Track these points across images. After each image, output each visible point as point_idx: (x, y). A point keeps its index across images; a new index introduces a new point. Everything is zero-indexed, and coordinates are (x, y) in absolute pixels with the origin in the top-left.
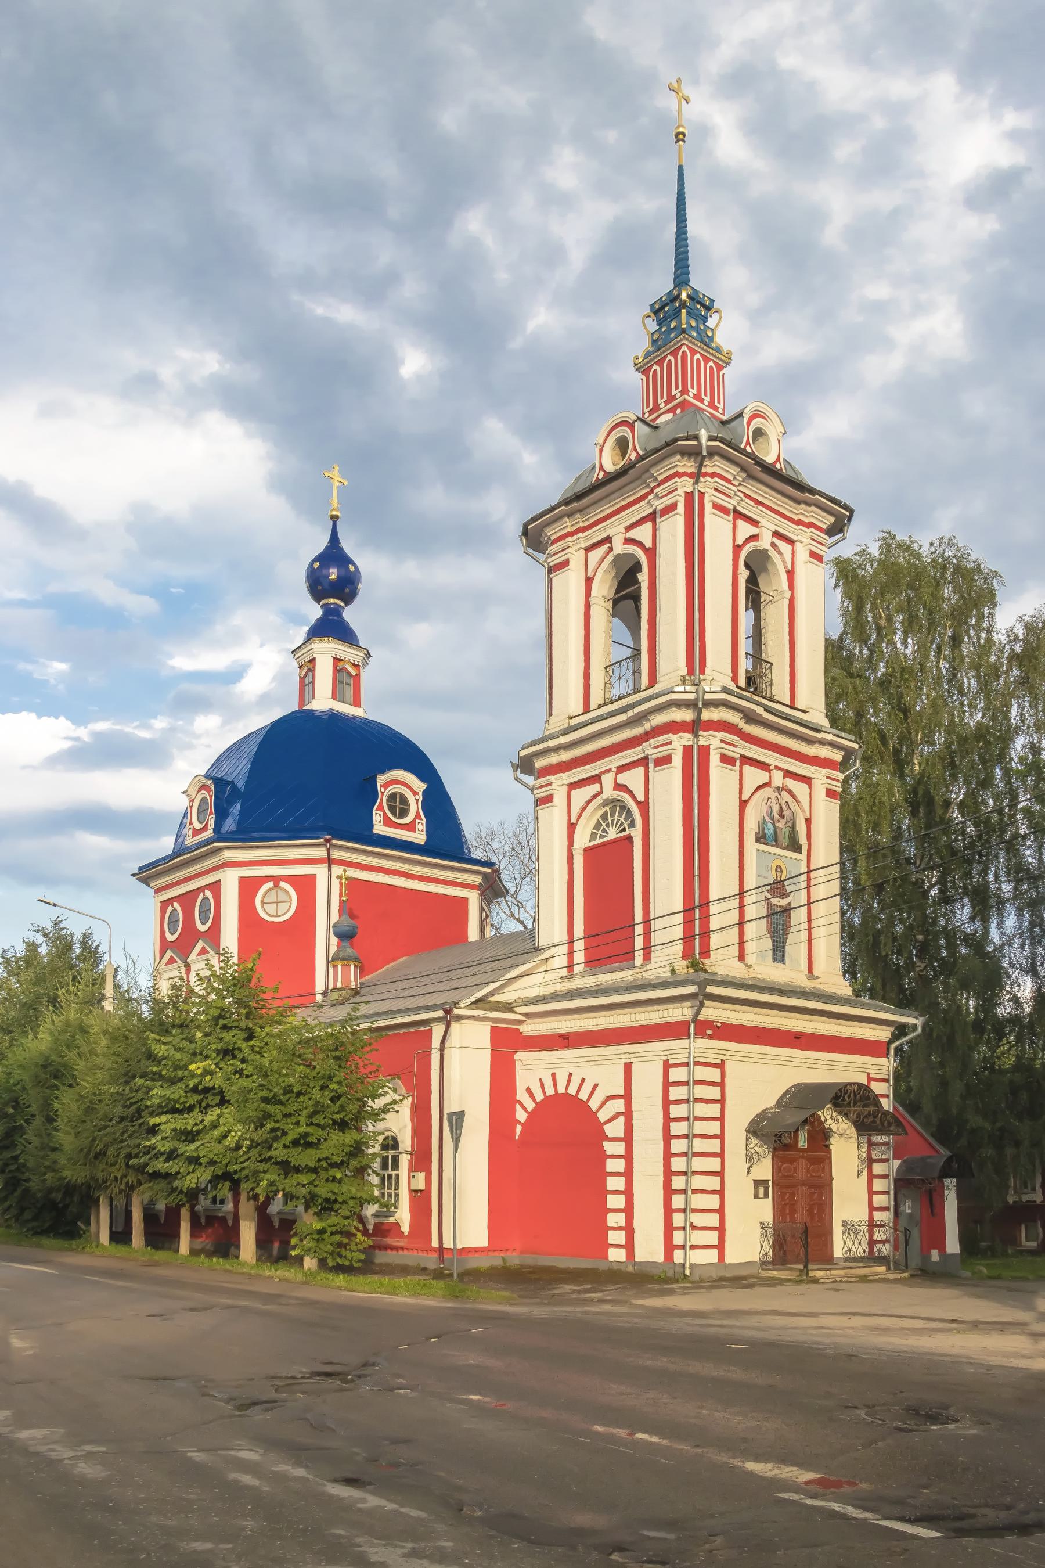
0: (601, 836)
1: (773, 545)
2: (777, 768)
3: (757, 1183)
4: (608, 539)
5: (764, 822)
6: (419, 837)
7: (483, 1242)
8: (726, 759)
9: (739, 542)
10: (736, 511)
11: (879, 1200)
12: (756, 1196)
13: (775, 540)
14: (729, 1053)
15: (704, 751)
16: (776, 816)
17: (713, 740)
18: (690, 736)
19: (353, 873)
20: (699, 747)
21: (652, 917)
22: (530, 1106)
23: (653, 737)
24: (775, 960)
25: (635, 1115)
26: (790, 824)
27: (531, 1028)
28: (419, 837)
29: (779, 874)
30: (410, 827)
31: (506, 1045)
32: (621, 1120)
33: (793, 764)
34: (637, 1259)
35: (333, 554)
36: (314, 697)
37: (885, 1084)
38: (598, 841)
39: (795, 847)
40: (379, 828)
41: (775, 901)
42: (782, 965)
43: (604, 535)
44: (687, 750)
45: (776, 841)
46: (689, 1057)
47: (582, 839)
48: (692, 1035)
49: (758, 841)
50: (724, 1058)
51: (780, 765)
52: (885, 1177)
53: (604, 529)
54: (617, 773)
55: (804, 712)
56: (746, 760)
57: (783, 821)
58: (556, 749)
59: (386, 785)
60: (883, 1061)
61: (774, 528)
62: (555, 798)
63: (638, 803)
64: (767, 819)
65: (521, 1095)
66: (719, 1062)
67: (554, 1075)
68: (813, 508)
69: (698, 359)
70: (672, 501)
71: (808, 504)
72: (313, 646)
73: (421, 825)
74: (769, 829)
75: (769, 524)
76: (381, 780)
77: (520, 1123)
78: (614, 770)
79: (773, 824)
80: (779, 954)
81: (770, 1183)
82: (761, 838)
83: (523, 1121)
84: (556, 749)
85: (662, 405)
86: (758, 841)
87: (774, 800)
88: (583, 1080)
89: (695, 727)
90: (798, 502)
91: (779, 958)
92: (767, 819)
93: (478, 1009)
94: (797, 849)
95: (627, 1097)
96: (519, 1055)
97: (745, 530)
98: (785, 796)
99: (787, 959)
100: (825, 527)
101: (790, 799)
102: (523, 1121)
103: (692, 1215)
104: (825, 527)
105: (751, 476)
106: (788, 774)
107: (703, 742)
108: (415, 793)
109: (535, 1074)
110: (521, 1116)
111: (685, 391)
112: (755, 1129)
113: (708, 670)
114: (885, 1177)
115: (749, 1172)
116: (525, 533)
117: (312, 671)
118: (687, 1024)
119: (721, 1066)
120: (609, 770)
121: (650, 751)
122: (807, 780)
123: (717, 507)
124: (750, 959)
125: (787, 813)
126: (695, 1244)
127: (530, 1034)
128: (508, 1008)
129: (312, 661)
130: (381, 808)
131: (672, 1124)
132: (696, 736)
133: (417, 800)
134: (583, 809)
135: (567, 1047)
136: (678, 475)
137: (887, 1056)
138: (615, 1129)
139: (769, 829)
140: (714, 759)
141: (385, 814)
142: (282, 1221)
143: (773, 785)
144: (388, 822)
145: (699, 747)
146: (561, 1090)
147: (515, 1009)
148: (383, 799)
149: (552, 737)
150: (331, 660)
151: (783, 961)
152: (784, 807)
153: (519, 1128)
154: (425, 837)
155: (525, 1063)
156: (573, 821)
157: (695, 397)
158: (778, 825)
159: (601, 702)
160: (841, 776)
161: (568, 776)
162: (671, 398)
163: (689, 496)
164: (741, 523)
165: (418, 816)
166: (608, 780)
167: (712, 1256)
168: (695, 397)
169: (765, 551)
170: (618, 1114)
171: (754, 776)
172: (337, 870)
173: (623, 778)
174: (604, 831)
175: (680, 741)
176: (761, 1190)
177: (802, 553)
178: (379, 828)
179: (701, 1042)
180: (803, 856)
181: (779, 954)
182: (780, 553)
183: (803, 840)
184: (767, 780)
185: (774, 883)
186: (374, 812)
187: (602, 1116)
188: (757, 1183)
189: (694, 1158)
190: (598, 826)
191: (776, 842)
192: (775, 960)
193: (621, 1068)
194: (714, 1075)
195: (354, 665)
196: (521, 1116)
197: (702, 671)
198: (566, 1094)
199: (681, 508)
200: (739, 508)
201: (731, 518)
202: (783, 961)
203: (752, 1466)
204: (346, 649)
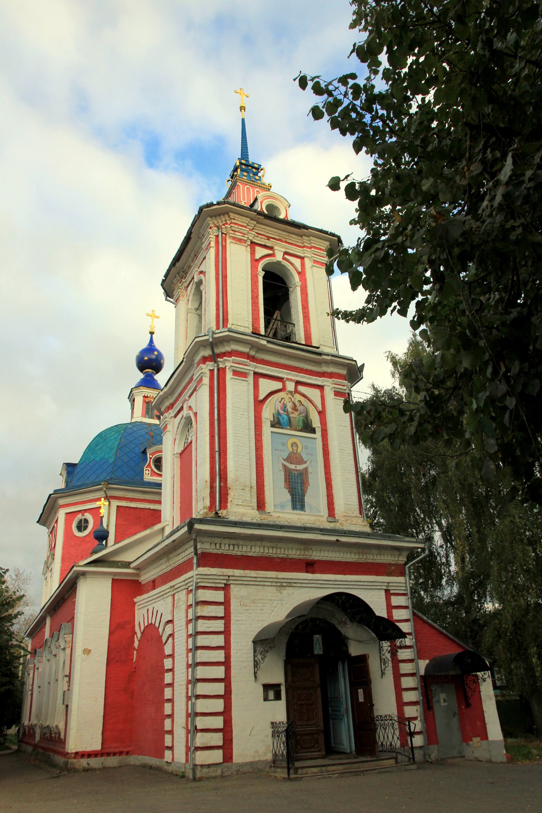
1: (284, 258)
2: (291, 380)
3: (267, 687)
5: (279, 413)
10: (252, 242)
11: (408, 697)
12: (266, 699)
13: (286, 256)
15: (222, 372)
16: (290, 410)
17: (228, 363)
19: (124, 504)
20: (219, 370)
24: (294, 508)
26: (303, 415)
29: (295, 448)
34: (221, 761)
37: (403, 598)
39: (308, 427)
42: (303, 512)
45: (291, 427)
48: (195, 565)
49: (273, 426)
51: (289, 377)
52: (413, 675)
55: (318, 348)
59: (152, 454)
60: (401, 579)
61: (284, 250)
64: (281, 412)
66: (223, 586)
76: (149, 452)
79: (288, 415)
80: (298, 502)
86: (273, 426)
87: (287, 400)
91: (298, 507)
94: (313, 431)
97: (260, 252)
98: (298, 397)
99: (307, 507)
104: (324, 248)
106: (298, 383)
112: (263, 642)
114: (413, 675)
122: (321, 388)
124: (269, 506)
125: (300, 408)
130: (149, 465)
131: (222, 644)
137: (403, 574)
140: (229, 375)
141: (152, 470)
142: (43, 735)
151: (302, 508)
152: (298, 404)
158: (291, 415)
164: (258, 248)
169: (279, 263)
172: (115, 503)
176: (271, 694)
180: (318, 435)
181: (298, 502)
183: (316, 423)
188: (267, 687)
191: (290, 424)
192: (294, 508)
194: (219, 596)
200: (254, 240)
202: (302, 508)
204: (150, 391)
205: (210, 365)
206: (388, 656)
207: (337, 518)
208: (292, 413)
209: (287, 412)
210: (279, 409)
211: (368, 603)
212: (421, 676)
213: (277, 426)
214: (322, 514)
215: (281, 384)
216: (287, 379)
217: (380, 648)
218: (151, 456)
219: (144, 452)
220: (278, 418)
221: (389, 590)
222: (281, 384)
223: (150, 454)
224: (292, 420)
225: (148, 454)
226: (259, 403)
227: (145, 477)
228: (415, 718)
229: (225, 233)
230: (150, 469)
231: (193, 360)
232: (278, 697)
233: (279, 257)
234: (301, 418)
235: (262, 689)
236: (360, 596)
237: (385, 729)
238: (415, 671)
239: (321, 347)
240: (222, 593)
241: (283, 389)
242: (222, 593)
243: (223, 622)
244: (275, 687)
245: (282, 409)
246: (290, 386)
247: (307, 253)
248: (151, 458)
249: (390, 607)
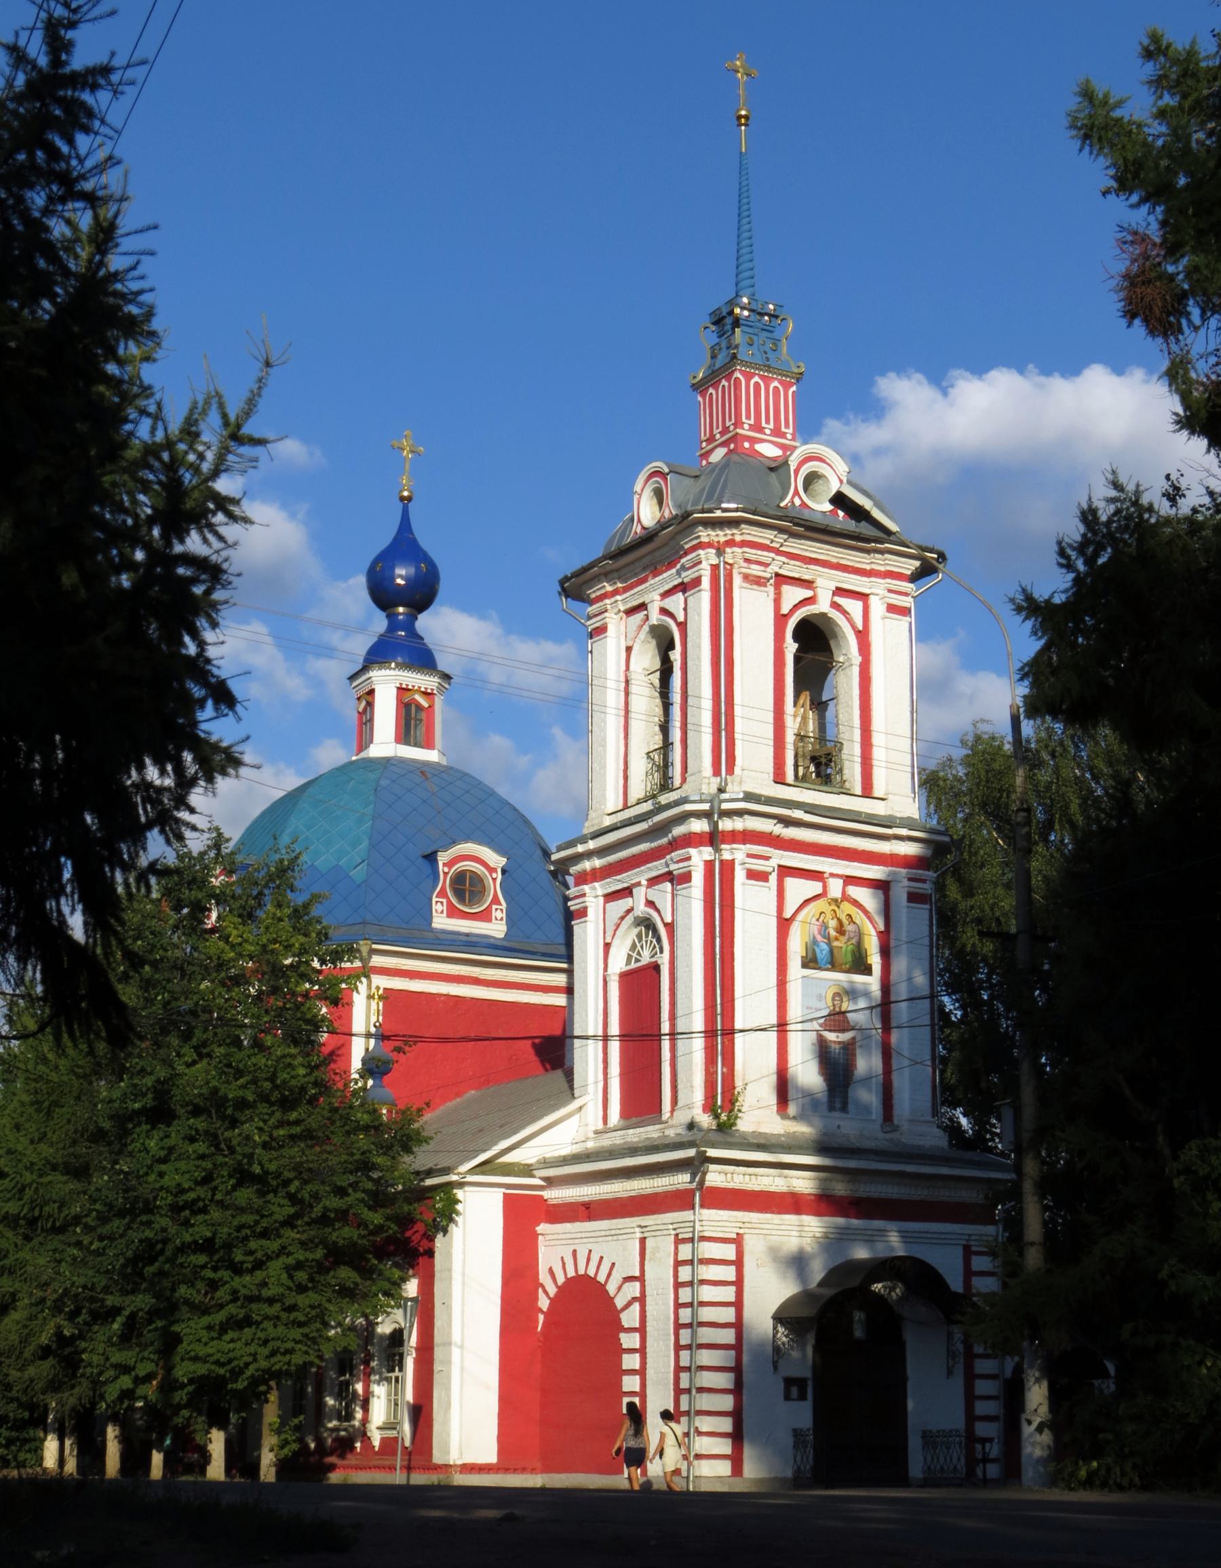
0: (637, 961)
3: (789, 1382)
4: (642, 607)
5: (815, 942)
6: (496, 928)
7: (488, 1454)
8: (753, 875)
9: (785, 610)
13: (837, 599)
14: (747, 1225)
15: (728, 868)
17: (737, 853)
18: (710, 849)
20: (722, 862)
21: (879, 1009)
22: (552, 1291)
23: (676, 849)
25: (648, 1299)
26: (854, 941)
27: (555, 1195)
28: (496, 928)
30: (485, 916)
31: (523, 1218)
32: (636, 1306)
33: (859, 868)
35: (404, 544)
36: (371, 741)
38: (633, 965)
40: (441, 921)
41: (831, 1036)
42: (843, 1115)
43: (640, 601)
44: (709, 865)
46: (693, 1232)
47: (618, 963)
48: (697, 1206)
49: (805, 965)
50: (741, 1231)
53: (640, 593)
54: (649, 886)
56: (785, 871)
57: (843, 939)
58: (589, 855)
59: (449, 864)
62: (590, 912)
63: (666, 925)
64: (819, 938)
65: (544, 1277)
66: (734, 1236)
67: (574, 1252)
68: (887, 556)
69: (757, 384)
70: (696, 574)
71: (882, 552)
72: (371, 674)
73: (499, 913)
74: (823, 951)
75: (827, 582)
76: (443, 858)
77: (541, 1311)
78: (644, 882)
79: (829, 944)
81: (810, 1383)
82: (810, 962)
83: (545, 1309)
84: (589, 855)
85: (718, 436)
86: (805, 965)
87: (829, 915)
88: (602, 1258)
89: (713, 839)
90: (868, 551)
91: (838, 1105)
92: (819, 938)
93: (483, 1173)
94: (867, 970)
95: (641, 1279)
96: (542, 1228)
97: (792, 595)
98: (847, 908)
100: (909, 573)
101: (854, 911)
102: (545, 1309)
103: (698, 1419)
105: (793, 535)
106: (850, 880)
107: (727, 856)
108: (492, 870)
109: (559, 1251)
110: (544, 1303)
111: (738, 423)
113: (737, 770)
115: (775, 1367)
116: (564, 589)
117: (370, 705)
118: (692, 1192)
119: (738, 1241)
120: (639, 884)
121: (673, 867)
123: (746, 577)
125: (849, 928)
126: (699, 1452)
127: (555, 1202)
128: (527, 1170)
129: (371, 692)
132: (718, 850)
133: (494, 880)
134: (618, 926)
135: (590, 1218)
136: (701, 546)
138: (630, 1318)
139: (823, 951)
140: (740, 875)
143: (829, 896)
144: (453, 912)
145: (722, 862)
146: (581, 1271)
147: (535, 1172)
148: (444, 881)
149: (583, 840)
150: (395, 691)
152: (845, 922)
153: (541, 1318)
154: (504, 928)
155: (548, 1237)
156: (608, 940)
157: (752, 428)
159: (642, 795)
160: (931, 874)
161: (602, 887)
162: (725, 430)
163: (715, 568)
165: (496, 901)
166: (640, 894)
167: (724, 1468)
168: (752, 428)
169: (824, 615)
170: (634, 1299)
171: (798, 889)
173: (653, 894)
174: (639, 954)
175: (699, 856)
176: (794, 1391)
177: (877, 607)
178: (441, 921)
179: (708, 1214)
182: (844, 613)
184: (819, 890)
185: (829, 1015)
186: (434, 899)
187: (619, 1302)
188: (789, 1382)
189: (700, 1351)
190: (634, 947)
193: (637, 1242)
194: (729, 1252)
195: (425, 694)
196: (544, 1303)
197: (730, 770)
198: (586, 1276)
199: (706, 583)
201: (771, 589)
202: (844, 1108)
203: (336, 1503)
205: (707, 853)
206: (960, 1347)
207: (896, 1122)
208: (836, 939)
209: (829, 938)
210: (816, 932)
211: (936, 1266)
212: (1006, 1381)
213: (811, 965)
214: (874, 1117)
215: (820, 884)
216: (832, 875)
217: (950, 1336)
218: (446, 870)
219: (431, 858)
220: (814, 951)
221: (970, 1246)
222: (820, 884)
223: (445, 865)
224: (836, 951)
225: (441, 864)
226: (784, 925)
227: (435, 920)
228: (990, 1440)
229: (731, 561)
230: (444, 901)
231: (670, 843)
232: (802, 1397)
233: (823, 605)
234: (850, 947)
235: (782, 1386)
236: (928, 1260)
237: (948, 1448)
238: (997, 1372)
239: (890, 797)
240: (733, 1247)
241: (824, 894)
242: (733, 1247)
243: (733, 1288)
244: (800, 1383)
245: (820, 933)
246: (835, 888)
247: (878, 590)
248: (446, 874)
249: (968, 1273)
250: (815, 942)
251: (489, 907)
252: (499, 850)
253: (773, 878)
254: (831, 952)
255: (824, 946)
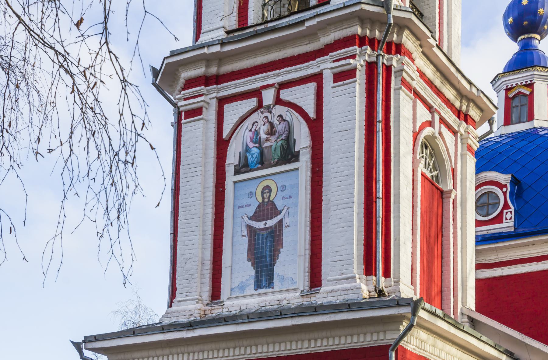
41: (259, 225)
42: (270, 290)
57: (273, 138)
64: (251, 145)
79: (260, 148)
91: (264, 283)
92: (251, 145)
152: (276, 122)
165: (506, 206)
208: (267, 140)
210: (249, 140)
213: (243, 170)
220: (246, 157)
224: (266, 151)
226: (222, 145)
245: (252, 141)
250: (247, 149)
251: (501, 212)
252: (504, 172)
253: (519, 107)
254: (262, 153)
255: (256, 151)
